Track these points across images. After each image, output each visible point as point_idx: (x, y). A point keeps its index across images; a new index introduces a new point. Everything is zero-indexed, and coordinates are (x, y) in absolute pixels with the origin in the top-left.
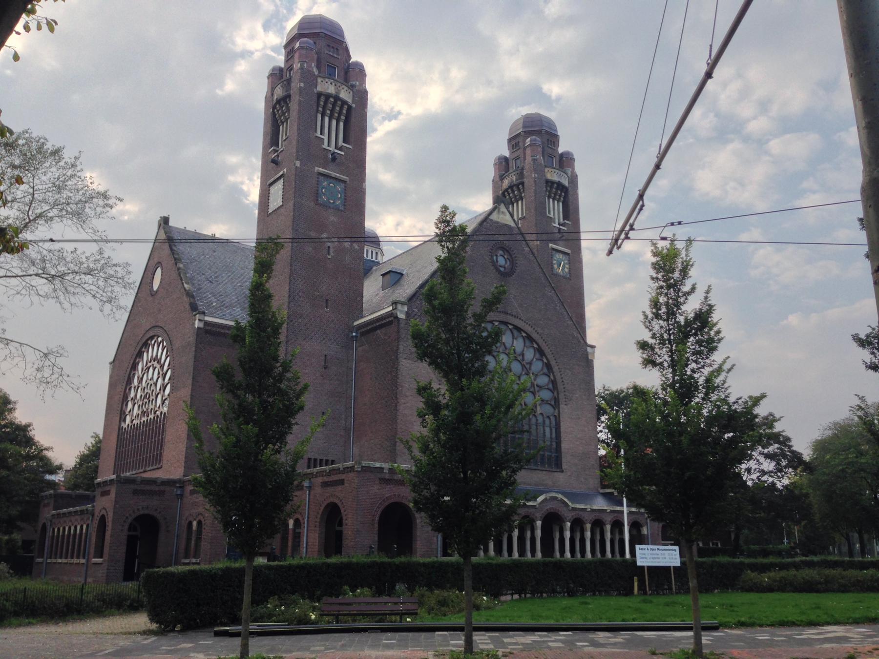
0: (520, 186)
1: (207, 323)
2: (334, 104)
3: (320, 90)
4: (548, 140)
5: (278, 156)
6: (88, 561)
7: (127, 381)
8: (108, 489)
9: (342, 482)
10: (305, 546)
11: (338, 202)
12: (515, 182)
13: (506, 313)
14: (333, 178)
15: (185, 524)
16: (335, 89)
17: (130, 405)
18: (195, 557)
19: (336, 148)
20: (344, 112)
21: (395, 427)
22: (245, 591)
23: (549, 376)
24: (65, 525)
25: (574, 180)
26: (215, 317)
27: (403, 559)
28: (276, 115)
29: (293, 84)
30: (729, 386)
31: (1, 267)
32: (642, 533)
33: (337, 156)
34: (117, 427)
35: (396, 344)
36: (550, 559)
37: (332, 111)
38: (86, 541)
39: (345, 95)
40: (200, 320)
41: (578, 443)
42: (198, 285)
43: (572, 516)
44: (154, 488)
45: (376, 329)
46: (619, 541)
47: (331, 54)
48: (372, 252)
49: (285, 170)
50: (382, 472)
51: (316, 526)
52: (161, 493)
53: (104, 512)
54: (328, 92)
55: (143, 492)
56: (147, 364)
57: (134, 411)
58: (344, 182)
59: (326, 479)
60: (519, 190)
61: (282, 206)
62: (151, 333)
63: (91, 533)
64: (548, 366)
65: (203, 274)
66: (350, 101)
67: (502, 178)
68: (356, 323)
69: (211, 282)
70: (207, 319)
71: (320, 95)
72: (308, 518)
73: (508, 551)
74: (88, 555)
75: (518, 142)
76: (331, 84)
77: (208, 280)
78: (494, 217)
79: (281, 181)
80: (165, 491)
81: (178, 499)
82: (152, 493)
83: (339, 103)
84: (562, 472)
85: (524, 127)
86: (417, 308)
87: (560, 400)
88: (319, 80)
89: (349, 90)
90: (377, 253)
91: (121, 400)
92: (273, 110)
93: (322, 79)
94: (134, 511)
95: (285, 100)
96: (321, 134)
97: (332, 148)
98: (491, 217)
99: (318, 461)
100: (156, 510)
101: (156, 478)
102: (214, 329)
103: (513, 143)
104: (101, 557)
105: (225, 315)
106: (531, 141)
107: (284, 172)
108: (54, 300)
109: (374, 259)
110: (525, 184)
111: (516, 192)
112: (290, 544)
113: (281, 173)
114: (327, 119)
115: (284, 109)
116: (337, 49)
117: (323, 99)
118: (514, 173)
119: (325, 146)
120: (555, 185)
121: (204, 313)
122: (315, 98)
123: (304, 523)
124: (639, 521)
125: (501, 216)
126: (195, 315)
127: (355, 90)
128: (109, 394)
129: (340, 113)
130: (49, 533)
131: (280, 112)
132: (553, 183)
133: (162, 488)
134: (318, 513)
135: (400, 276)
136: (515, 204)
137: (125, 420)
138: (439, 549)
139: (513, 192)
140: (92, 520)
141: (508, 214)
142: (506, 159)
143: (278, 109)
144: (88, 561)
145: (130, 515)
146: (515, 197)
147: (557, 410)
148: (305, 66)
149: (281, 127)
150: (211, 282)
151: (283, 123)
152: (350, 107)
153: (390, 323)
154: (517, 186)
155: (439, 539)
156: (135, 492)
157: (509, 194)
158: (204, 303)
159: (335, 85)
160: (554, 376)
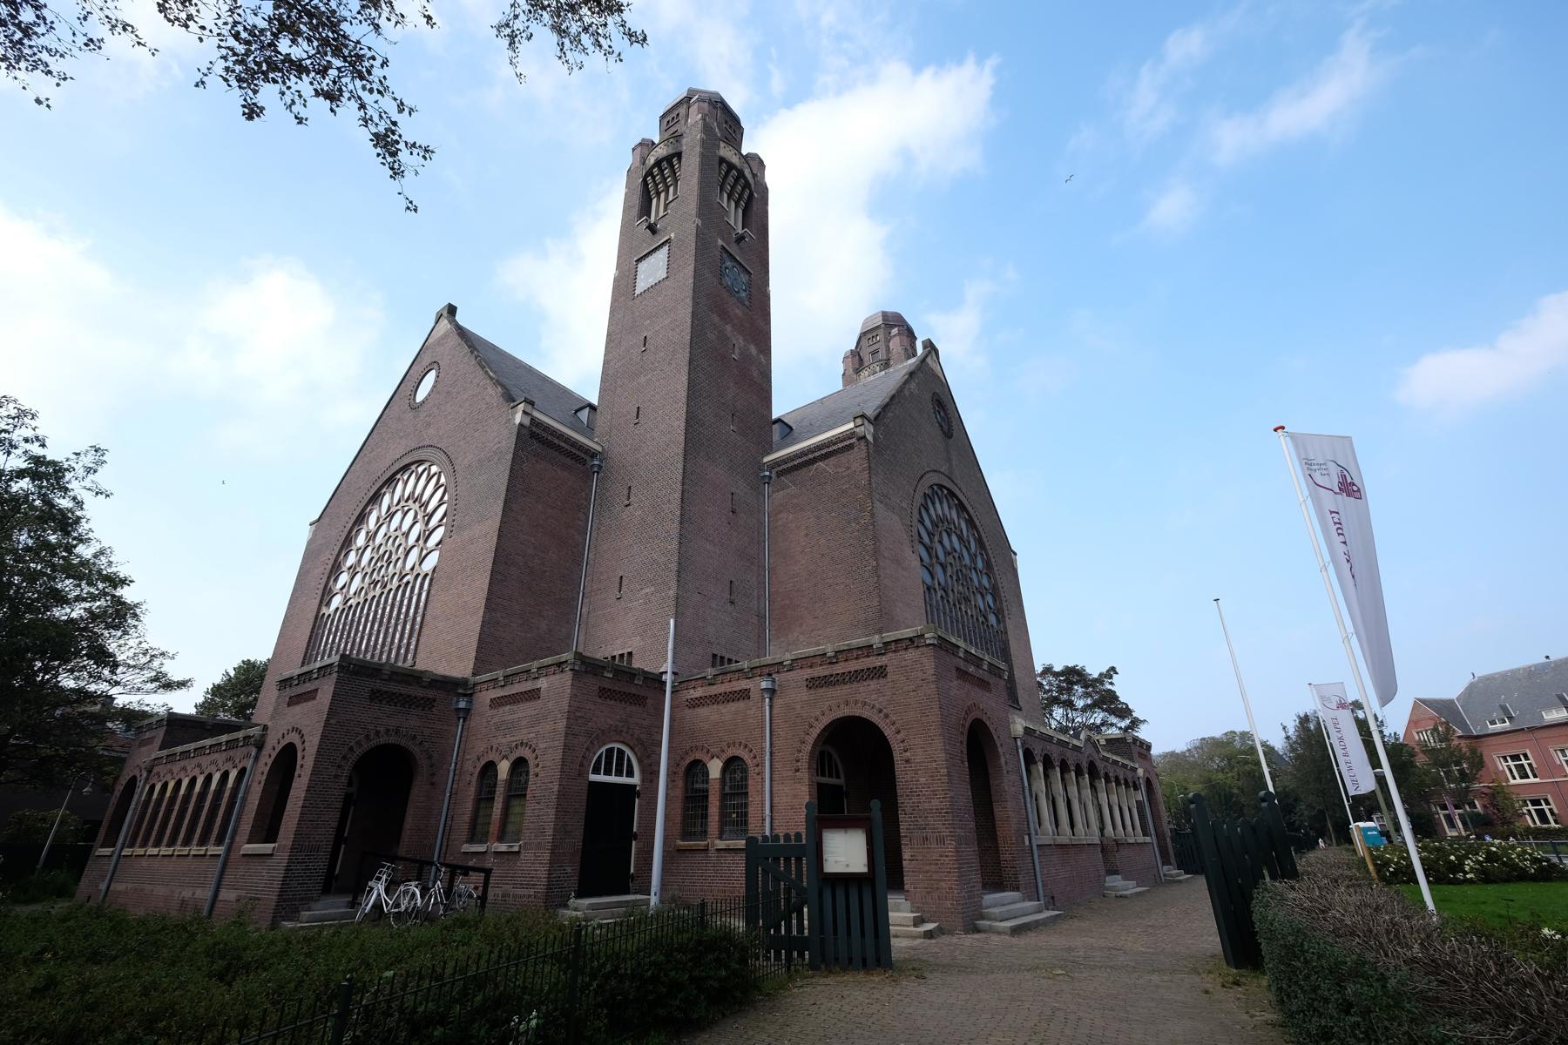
7: (345, 541)
8: (313, 688)
9: (880, 672)
15: (473, 768)
17: (344, 578)
18: (501, 839)
24: (182, 775)
27: (804, 837)
34: (312, 616)
45: (815, 460)
52: (429, 703)
53: (294, 738)
55: (392, 698)
57: (349, 585)
61: (667, 278)
63: (248, 788)
64: (988, 565)
68: (766, 459)
70: (536, 414)
72: (771, 754)
79: (666, 248)
80: (434, 701)
81: (459, 718)
82: (407, 702)
84: (1020, 710)
91: (328, 571)
92: (645, 180)
95: (671, 161)
123: (760, 765)
128: (294, 587)
130: (140, 794)
133: (430, 694)
135: (788, 430)
137: (328, 604)
140: (257, 759)
145: (359, 744)
149: (654, 201)
151: (658, 194)
153: (851, 447)
156: (376, 696)
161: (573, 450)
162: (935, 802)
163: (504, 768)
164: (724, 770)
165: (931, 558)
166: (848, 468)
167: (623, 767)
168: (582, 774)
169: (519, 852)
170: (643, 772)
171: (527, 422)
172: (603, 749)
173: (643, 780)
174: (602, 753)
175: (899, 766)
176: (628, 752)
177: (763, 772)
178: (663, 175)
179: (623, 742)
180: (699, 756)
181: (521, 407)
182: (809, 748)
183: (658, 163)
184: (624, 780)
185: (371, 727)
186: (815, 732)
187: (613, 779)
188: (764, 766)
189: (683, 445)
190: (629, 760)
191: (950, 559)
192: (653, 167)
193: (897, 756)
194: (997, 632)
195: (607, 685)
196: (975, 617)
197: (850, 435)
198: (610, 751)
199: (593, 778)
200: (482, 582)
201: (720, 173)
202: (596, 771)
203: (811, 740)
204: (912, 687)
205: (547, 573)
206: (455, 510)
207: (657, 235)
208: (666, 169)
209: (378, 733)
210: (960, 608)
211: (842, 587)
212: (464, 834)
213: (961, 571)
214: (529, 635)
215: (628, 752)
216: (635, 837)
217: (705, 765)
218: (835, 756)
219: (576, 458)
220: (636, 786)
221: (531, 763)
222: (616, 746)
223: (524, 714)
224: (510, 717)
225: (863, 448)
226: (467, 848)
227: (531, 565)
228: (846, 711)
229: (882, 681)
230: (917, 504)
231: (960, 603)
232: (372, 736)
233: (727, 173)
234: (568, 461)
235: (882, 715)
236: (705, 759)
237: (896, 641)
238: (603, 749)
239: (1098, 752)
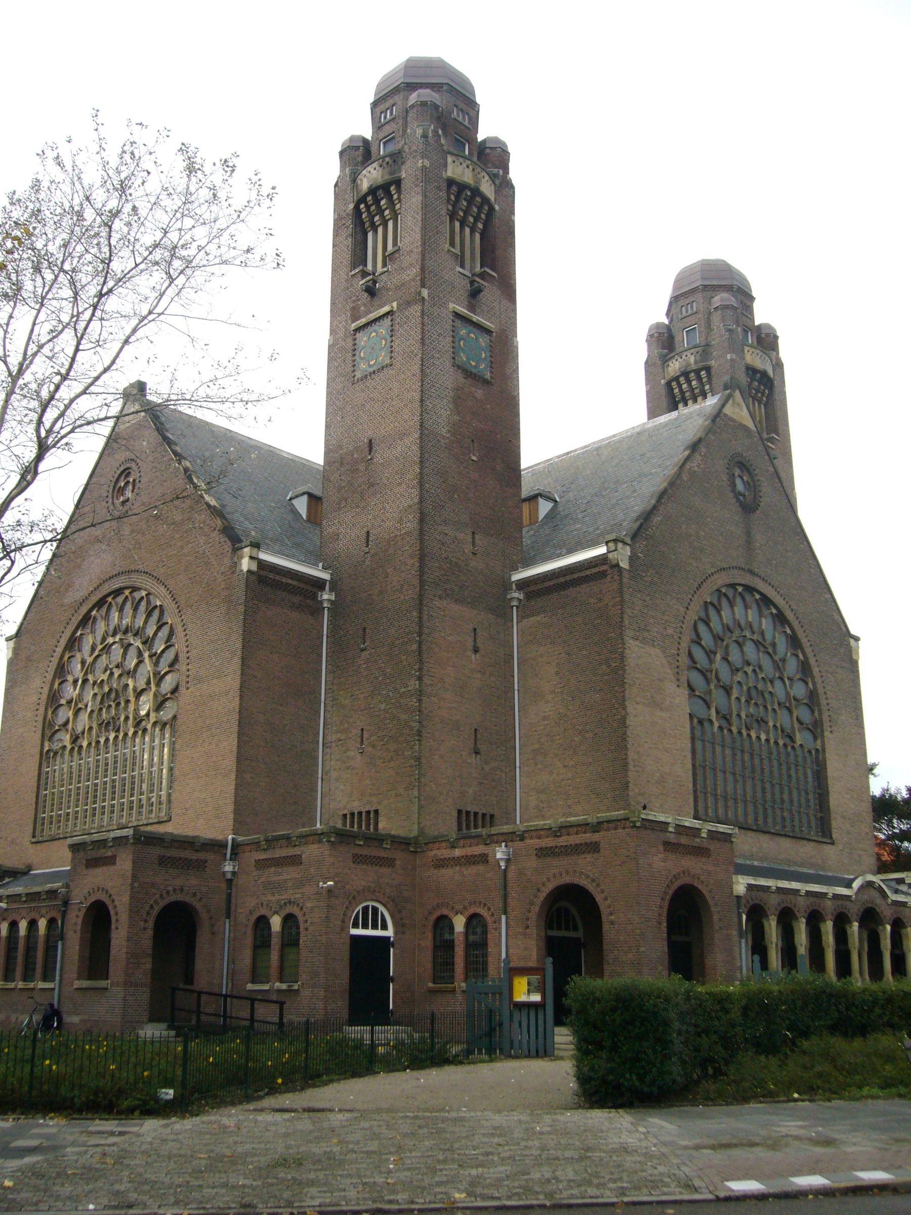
0: (703, 373)
1: (262, 564)
2: (689, 381)
9: (594, 847)
11: (482, 366)
12: (694, 367)
13: (751, 572)
21: (624, 757)
23: (806, 683)
25: (778, 365)
28: (361, 214)
35: (619, 611)
40: (251, 558)
41: (848, 797)
44: (188, 854)
48: (844, 968)
49: (395, 304)
50: (666, 831)
51: (527, 927)
56: (104, 639)
59: (549, 842)
60: (699, 379)
62: (116, 584)
64: (805, 668)
67: (665, 360)
68: (517, 577)
76: (468, 167)
79: (387, 322)
80: (206, 861)
82: (186, 865)
84: (833, 844)
85: (703, 279)
87: (825, 724)
89: (764, 356)
92: (357, 207)
93: (454, 158)
94: (161, 896)
99: (472, 814)
100: (195, 895)
101: (193, 837)
106: (722, 300)
117: (674, 384)
118: (692, 351)
125: (737, 410)
134: (532, 904)
136: (380, 230)
143: (370, 203)
146: (692, 390)
147: (819, 742)
149: (370, 235)
151: (375, 229)
153: (603, 574)
154: (697, 372)
155: (743, 951)
156: (163, 861)
159: (473, 170)
160: (814, 684)
162: (630, 956)
163: (276, 922)
164: (468, 924)
165: (708, 681)
166: (600, 600)
167: (377, 921)
168: (344, 928)
169: (298, 990)
171: (254, 567)
173: (396, 933)
174: (358, 912)
175: (606, 927)
176: (381, 908)
177: (500, 928)
178: (382, 216)
180: (445, 912)
181: (247, 550)
182: (537, 909)
183: (373, 191)
184: (379, 933)
185: (162, 887)
186: (543, 895)
187: (370, 932)
188: (500, 923)
189: (418, 589)
190: (382, 915)
191: (739, 677)
192: (367, 195)
193: (604, 918)
194: (810, 752)
195: (358, 851)
196: (772, 742)
197: (602, 559)
198: (365, 909)
199: (354, 932)
200: (230, 743)
202: (355, 925)
203: (539, 901)
204: (619, 862)
206: (188, 658)
207: (377, 301)
208: (382, 199)
209: (168, 892)
210: (749, 735)
211: (591, 735)
212: (248, 976)
213: (755, 687)
215: (381, 908)
216: (393, 979)
217: (451, 920)
218: (574, 911)
220: (389, 938)
221: (301, 919)
222: (371, 904)
223: (289, 877)
224: (276, 878)
225: (616, 577)
226: (250, 986)
228: (567, 879)
229: (596, 855)
230: (692, 616)
231: (748, 729)
232: (165, 895)
233: (458, 197)
235: (594, 884)
236: (451, 915)
237: (609, 822)
238: (360, 907)
239: (884, 895)
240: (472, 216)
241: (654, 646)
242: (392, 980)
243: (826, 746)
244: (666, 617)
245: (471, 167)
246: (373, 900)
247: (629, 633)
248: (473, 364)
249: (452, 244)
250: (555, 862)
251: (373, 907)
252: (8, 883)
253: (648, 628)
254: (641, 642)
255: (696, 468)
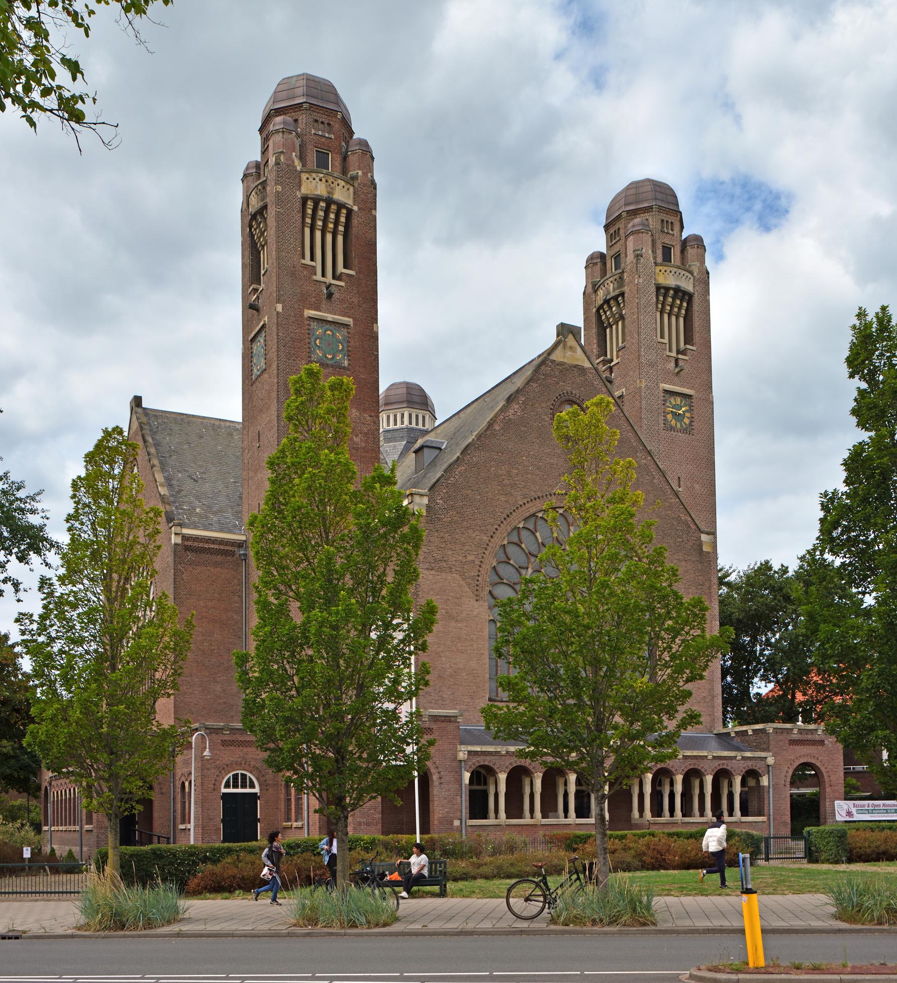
0: (620, 298)
1: (185, 538)
2: (327, 211)
3: (305, 192)
4: (663, 221)
5: (258, 297)
6: (81, 828)
10: (306, 808)
12: (612, 294)
14: (330, 322)
16: (326, 187)
19: (334, 278)
20: (343, 219)
22: (682, 389)
26: (235, 533)
29: (268, 188)
30: (87, 6)
31: (1, 893)
32: (761, 784)
33: (333, 289)
36: (254, 843)
37: (325, 220)
38: (74, 806)
39: (343, 194)
40: (176, 534)
42: (178, 486)
43: (511, 764)
46: (740, 794)
47: (320, 133)
48: (417, 416)
54: (316, 193)
58: (346, 326)
60: (618, 304)
65: (185, 470)
66: (349, 202)
69: (195, 480)
70: (185, 531)
71: (305, 200)
73: (699, 811)
74: (81, 823)
75: (619, 229)
76: (321, 180)
77: (192, 479)
78: (557, 356)
83: (334, 207)
86: (442, 499)
88: (304, 176)
89: (348, 186)
90: (424, 417)
92: (250, 230)
93: (307, 175)
96: (661, 338)
97: (329, 279)
98: (553, 357)
102: (196, 544)
103: (612, 231)
104: (91, 824)
105: (212, 524)
106: (284, 122)
107: (265, 321)
108: (72, 511)
109: (420, 426)
110: (626, 295)
111: (614, 309)
112: (293, 807)
113: (262, 323)
114: (666, 317)
115: (261, 226)
116: (329, 124)
117: (310, 204)
119: (318, 277)
120: (672, 292)
121: (181, 525)
122: (298, 205)
124: (756, 769)
125: (569, 353)
126: (171, 528)
127: (356, 185)
129: (336, 223)
131: (258, 231)
132: (667, 289)
135: (437, 451)
136: (614, 327)
138: (464, 811)
139: (610, 308)
141: (579, 350)
142: (602, 256)
144: (81, 828)
148: (282, 159)
149: (262, 252)
150: (195, 480)
151: (263, 247)
152: (350, 212)
154: (615, 298)
156: (793, 742)
157: (605, 313)
158: (185, 509)
159: (327, 181)
161: (222, 547)
170: (260, 785)
171: (179, 540)
172: (231, 774)
173: (261, 790)
174: (229, 779)
176: (249, 774)
179: (243, 770)
190: (250, 779)
195: (226, 738)
201: (657, 307)
205: (215, 651)
214: (209, 697)
215: (249, 774)
219: (225, 553)
222: (240, 772)
227: (202, 647)
230: (501, 538)
234: (219, 558)
238: (231, 774)
240: (331, 222)
241: (451, 572)
242: (137, 823)
243: (314, 939)
244: (466, 548)
245: (324, 180)
246: (240, 769)
247: (463, 769)
248: (330, 357)
249: (662, 337)
250: (797, 748)
251: (242, 774)
252: (884, 930)
253: (446, 559)
254: (436, 571)
255: (511, 417)
